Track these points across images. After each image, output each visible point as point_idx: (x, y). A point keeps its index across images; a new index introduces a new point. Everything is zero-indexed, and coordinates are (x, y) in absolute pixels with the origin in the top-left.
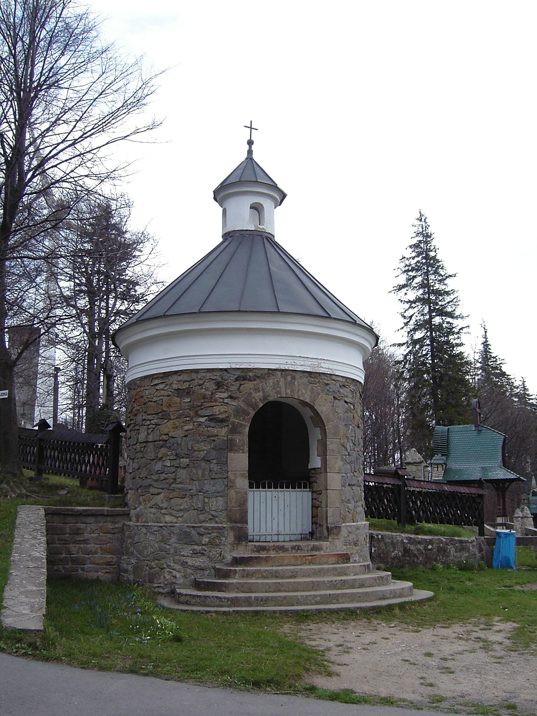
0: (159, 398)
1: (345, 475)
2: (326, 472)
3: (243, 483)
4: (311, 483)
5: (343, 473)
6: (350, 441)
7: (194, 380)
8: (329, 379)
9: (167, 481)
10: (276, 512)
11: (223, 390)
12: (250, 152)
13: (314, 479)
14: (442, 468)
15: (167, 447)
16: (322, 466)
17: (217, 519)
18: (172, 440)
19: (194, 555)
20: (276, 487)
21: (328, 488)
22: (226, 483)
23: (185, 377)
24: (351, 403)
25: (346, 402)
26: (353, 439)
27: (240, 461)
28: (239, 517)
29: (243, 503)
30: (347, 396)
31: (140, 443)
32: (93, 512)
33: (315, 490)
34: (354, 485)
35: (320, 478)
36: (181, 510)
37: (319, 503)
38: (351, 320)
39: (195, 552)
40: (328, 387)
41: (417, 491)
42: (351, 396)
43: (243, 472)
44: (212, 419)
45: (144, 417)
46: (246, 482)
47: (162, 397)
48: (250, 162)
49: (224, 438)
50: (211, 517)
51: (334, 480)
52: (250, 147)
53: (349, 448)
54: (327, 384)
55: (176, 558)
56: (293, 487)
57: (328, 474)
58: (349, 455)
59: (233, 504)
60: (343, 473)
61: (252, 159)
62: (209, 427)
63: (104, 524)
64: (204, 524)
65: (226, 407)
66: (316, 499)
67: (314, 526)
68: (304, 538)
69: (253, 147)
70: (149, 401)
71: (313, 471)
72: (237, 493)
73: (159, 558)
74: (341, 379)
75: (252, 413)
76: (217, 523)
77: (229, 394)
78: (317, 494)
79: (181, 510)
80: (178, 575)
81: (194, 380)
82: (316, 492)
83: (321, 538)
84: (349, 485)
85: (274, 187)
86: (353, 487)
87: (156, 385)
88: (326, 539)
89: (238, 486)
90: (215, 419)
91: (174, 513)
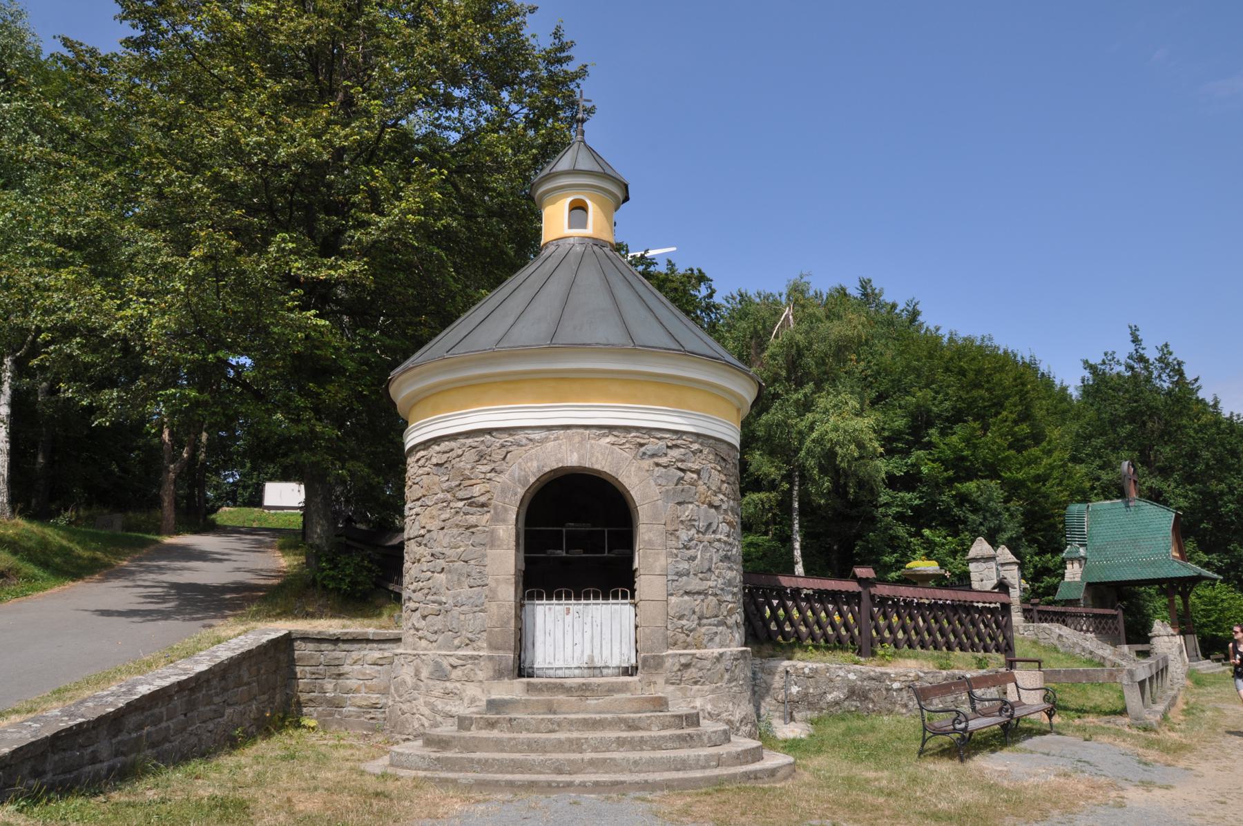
40: (643, 449)
54: (642, 445)
72: (499, 607)
75: (521, 491)
77: (493, 465)
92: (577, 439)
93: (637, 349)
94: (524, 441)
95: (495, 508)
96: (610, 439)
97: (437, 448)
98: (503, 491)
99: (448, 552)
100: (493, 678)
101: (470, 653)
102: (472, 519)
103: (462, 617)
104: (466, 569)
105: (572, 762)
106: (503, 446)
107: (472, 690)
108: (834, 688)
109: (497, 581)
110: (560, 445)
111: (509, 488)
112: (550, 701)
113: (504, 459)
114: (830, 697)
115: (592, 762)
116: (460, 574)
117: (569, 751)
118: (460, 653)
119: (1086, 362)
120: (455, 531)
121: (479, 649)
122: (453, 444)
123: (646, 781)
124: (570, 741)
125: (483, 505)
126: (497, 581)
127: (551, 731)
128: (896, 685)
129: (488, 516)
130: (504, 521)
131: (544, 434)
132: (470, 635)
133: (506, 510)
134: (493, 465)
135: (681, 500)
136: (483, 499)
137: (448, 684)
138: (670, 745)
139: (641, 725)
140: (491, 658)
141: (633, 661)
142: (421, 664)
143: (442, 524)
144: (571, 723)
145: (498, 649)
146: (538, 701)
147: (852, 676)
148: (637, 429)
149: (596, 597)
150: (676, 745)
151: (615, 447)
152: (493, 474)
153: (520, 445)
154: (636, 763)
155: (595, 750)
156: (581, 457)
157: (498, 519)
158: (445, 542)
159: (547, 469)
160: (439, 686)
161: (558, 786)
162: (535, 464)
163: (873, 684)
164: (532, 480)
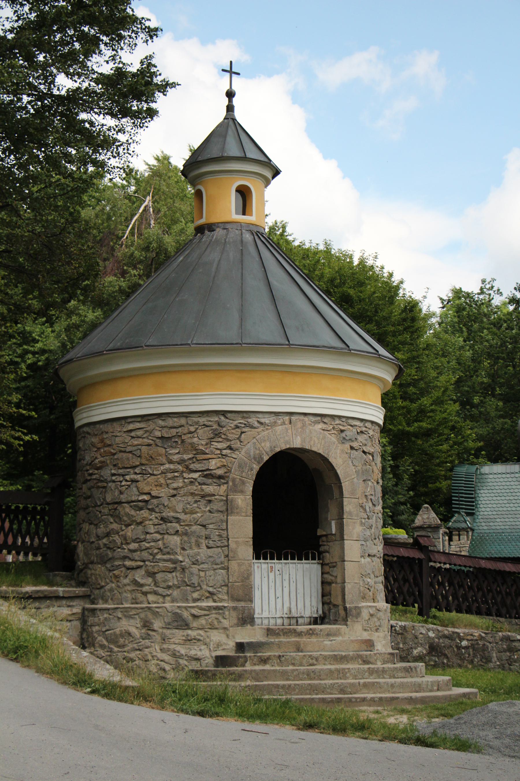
0: (135, 448)
1: (363, 543)
2: (342, 539)
3: (247, 551)
4: (320, 553)
5: (362, 537)
6: (370, 501)
7: (183, 426)
8: (345, 424)
9: (150, 551)
10: (282, 588)
11: (220, 439)
12: (230, 108)
13: (326, 548)
14: (468, 537)
15: (149, 509)
16: (336, 531)
17: (215, 598)
18: (155, 501)
19: (188, 642)
20: (279, 559)
21: (346, 559)
22: (226, 553)
23: (176, 421)
24: (369, 454)
25: (364, 452)
26: (373, 497)
27: (242, 526)
28: (244, 594)
29: (247, 576)
30: (366, 445)
31: (108, 504)
32: (46, 593)
33: (327, 561)
34: (374, 556)
35: (334, 548)
36: (169, 587)
37: (333, 578)
38: (263, 158)
39: (189, 638)
40: (343, 435)
41: (445, 569)
42: (370, 444)
43: (247, 540)
44: (206, 475)
45: (113, 471)
46: (250, 551)
47: (140, 447)
48: (231, 123)
49: (223, 498)
50: (208, 595)
51: (352, 549)
52: (230, 101)
53: (368, 510)
54: (342, 431)
55: (165, 646)
56: (300, 559)
57: (346, 542)
58: (368, 518)
59: (235, 579)
60: (362, 537)
61: (234, 120)
62: (204, 484)
63: (59, 608)
64: (199, 604)
65: (223, 460)
66: (328, 573)
67: (326, 607)
68: (315, 621)
69: (235, 100)
70: (121, 451)
71: (324, 539)
72: (239, 565)
73: (141, 648)
74: (358, 423)
75: (256, 468)
76: (215, 601)
77: (228, 443)
78: (330, 567)
79: (169, 587)
80: (167, 667)
81: (183, 426)
82: (328, 564)
83: (335, 622)
84: (369, 555)
85: (268, 163)
86: (373, 558)
87: (131, 431)
88: (345, 621)
89: (241, 557)
90: (210, 474)
91: (160, 590)
92: (299, 425)
93: (345, 350)
94: (256, 424)
95: (234, 480)
96: (321, 426)
97: (161, 423)
98: (240, 466)
99: (182, 516)
100: (238, 625)
101: (211, 604)
102: (209, 489)
103: (202, 574)
104: (204, 532)
105: (352, 685)
106: (237, 427)
107: (216, 636)
108: (417, 645)
109: (237, 542)
110: (287, 430)
111: (246, 464)
112: (298, 642)
113: (239, 438)
114: (415, 652)
115: (365, 685)
116: (199, 537)
117: (337, 679)
118: (204, 604)
119: (173, 85)
120: (190, 499)
121: (221, 600)
122: (183, 421)
123: (411, 697)
124: (338, 671)
125: (220, 477)
126: (237, 542)
127: (311, 665)
128: (464, 643)
129: (224, 488)
130: (242, 492)
131: (272, 418)
132: (211, 589)
133: (243, 483)
134: (228, 443)
135: (365, 478)
136: (220, 472)
137: (189, 632)
138: (400, 674)
139: (371, 660)
140: (235, 608)
141: (320, 612)
142: (150, 616)
143: (173, 492)
144: (325, 658)
145: (239, 600)
146: (288, 642)
147: (431, 634)
148: (340, 417)
149: (293, 558)
150: (403, 675)
151: (326, 432)
152: (228, 451)
153: (252, 427)
154: (392, 686)
155: (355, 677)
156: (303, 441)
157: (236, 489)
158: (180, 507)
159: (278, 450)
160: (179, 635)
161: (356, 701)
162: (268, 444)
163: (447, 642)
164: (266, 458)
